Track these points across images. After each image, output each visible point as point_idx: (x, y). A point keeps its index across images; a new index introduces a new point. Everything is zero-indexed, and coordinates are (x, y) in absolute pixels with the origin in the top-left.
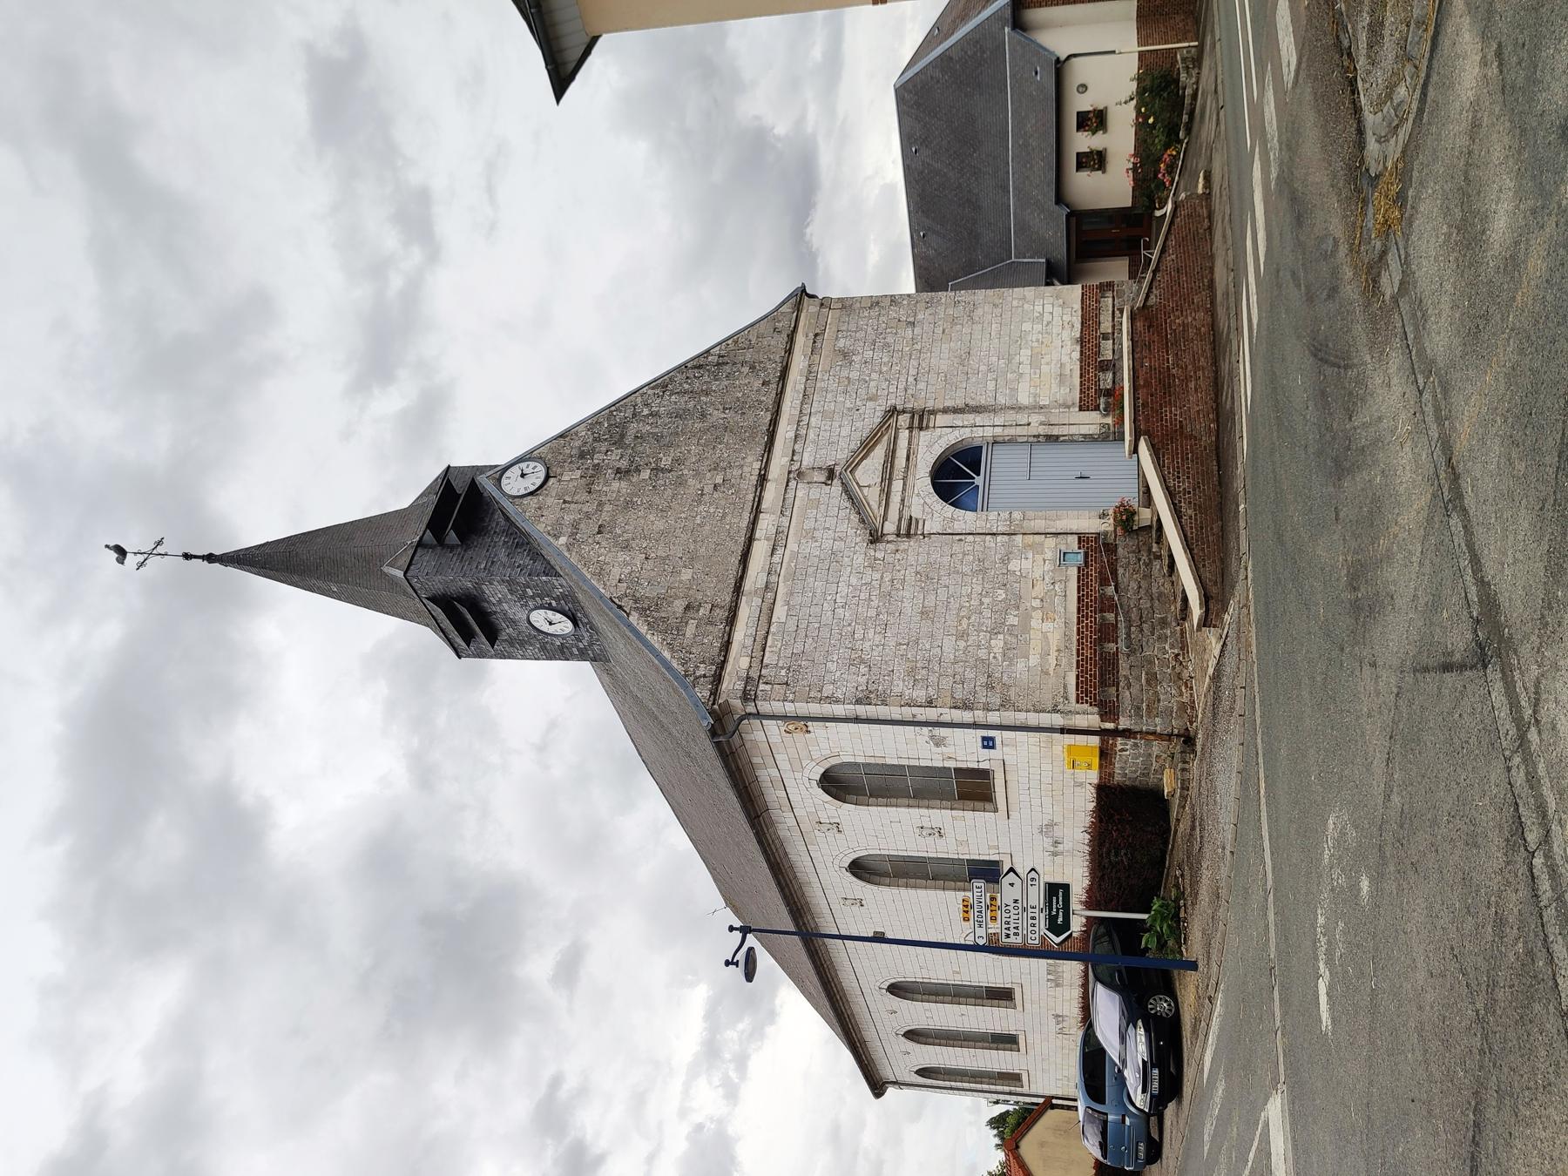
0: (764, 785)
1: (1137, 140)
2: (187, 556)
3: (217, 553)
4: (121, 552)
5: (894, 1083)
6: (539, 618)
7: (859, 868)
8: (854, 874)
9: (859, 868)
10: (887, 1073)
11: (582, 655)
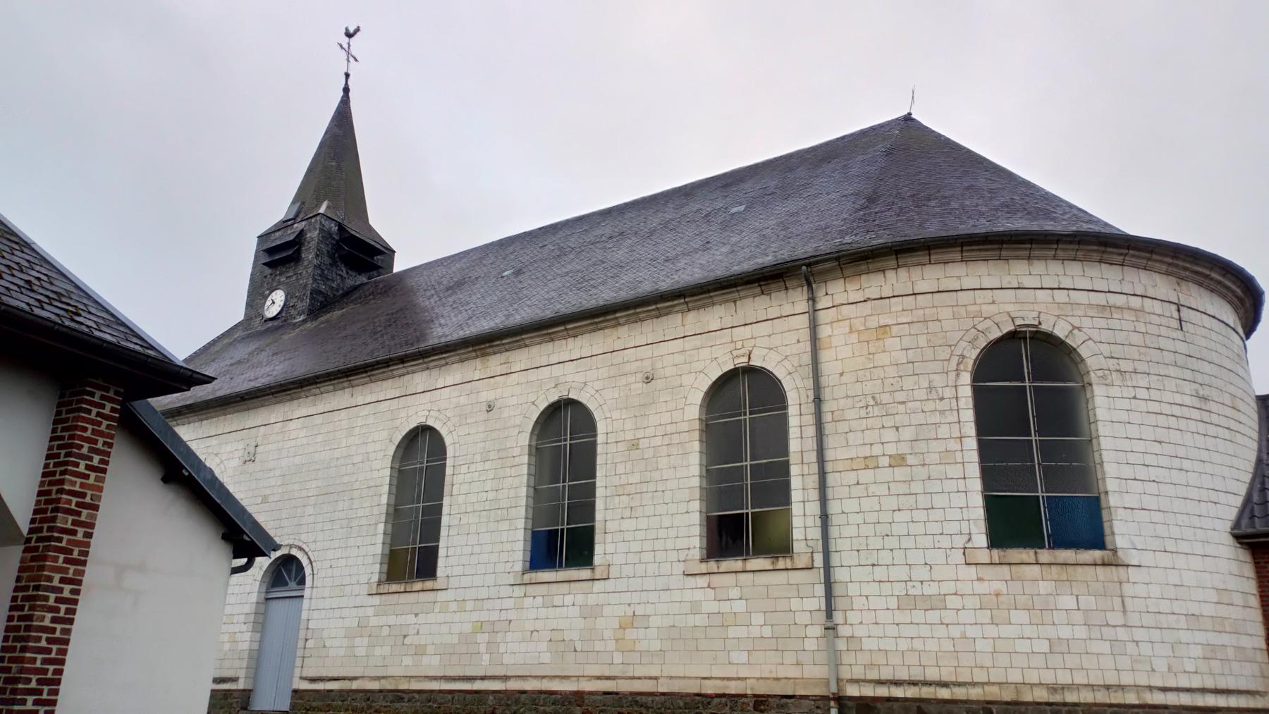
2: (347, 75)
11: (248, 319)
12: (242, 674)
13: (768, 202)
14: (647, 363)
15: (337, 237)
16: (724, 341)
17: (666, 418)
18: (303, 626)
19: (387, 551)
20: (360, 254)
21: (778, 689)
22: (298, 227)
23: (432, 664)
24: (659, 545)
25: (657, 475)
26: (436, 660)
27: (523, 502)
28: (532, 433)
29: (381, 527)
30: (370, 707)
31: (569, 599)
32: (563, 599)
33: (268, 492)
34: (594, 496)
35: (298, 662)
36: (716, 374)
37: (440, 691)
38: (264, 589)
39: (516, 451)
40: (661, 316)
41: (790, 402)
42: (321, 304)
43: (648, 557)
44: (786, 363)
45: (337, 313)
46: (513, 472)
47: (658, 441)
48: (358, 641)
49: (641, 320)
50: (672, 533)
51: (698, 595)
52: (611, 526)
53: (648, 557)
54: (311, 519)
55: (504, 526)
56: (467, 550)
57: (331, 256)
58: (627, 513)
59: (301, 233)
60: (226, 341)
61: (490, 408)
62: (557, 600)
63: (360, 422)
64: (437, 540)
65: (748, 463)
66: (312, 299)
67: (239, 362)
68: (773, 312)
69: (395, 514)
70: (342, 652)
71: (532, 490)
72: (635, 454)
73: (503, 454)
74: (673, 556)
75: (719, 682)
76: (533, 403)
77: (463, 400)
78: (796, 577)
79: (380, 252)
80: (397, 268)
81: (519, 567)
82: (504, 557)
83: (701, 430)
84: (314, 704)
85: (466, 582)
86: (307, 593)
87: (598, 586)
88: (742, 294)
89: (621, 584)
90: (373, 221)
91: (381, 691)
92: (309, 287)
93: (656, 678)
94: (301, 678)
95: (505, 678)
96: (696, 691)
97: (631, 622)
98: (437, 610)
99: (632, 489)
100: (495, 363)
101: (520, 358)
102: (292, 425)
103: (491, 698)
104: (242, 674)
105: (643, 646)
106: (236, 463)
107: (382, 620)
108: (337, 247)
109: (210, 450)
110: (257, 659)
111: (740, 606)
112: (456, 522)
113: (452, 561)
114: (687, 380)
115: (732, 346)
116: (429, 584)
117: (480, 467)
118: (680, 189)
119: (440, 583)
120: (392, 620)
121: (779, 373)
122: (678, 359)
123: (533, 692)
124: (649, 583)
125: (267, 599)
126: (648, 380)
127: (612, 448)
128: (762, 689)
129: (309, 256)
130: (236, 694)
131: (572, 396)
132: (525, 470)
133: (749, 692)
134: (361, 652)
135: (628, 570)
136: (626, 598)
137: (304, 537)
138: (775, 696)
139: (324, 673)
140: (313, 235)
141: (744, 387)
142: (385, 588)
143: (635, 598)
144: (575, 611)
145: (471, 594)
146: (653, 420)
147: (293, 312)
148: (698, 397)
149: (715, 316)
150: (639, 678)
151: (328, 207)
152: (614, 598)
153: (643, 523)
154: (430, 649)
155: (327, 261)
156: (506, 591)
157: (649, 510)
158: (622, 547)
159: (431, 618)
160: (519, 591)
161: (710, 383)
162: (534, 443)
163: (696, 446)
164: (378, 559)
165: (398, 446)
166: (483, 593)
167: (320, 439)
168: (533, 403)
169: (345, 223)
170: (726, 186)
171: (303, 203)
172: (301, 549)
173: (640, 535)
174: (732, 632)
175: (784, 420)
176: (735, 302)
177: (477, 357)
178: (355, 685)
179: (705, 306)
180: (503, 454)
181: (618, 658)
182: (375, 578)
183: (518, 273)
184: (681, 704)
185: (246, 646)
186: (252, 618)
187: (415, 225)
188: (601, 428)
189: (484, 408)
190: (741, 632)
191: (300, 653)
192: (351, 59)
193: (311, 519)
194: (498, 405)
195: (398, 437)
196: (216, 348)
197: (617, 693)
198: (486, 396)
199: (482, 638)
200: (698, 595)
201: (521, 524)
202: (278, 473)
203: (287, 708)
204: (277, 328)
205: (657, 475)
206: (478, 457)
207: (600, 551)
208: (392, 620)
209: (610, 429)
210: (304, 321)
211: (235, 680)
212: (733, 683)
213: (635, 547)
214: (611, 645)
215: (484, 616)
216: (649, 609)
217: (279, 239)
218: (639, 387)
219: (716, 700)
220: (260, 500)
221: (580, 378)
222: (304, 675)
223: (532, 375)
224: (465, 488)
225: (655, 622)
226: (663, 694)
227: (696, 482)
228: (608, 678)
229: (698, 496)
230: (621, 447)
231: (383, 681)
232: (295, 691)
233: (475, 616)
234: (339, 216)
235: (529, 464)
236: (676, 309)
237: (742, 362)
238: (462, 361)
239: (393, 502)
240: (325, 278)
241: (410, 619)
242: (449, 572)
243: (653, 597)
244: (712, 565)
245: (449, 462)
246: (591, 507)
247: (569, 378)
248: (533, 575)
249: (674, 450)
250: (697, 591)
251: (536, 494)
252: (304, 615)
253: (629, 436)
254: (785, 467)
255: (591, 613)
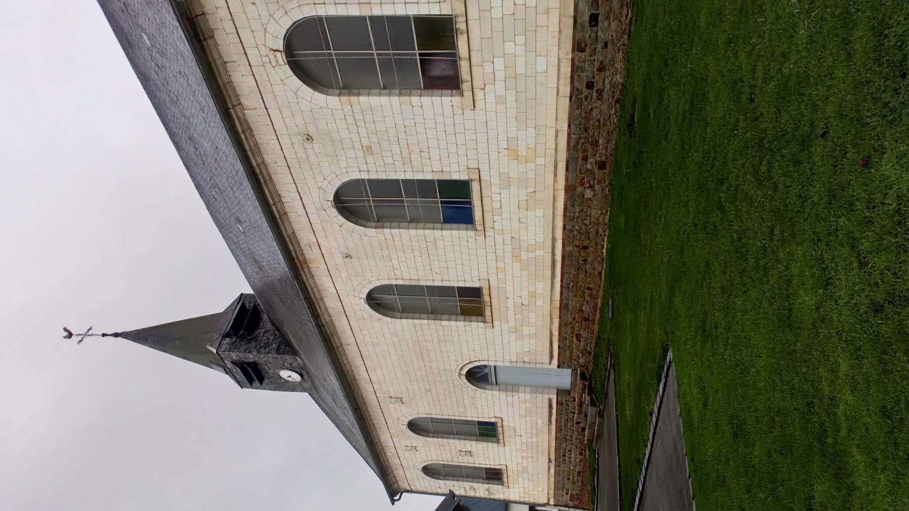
1: (584, 91)
2: (104, 335)
3: (120, 332)
4: (70, 335)
5: (407, 491)
6: (285, 374)
8: (425, 473)
9: (415, 426)
10: (403, 484)
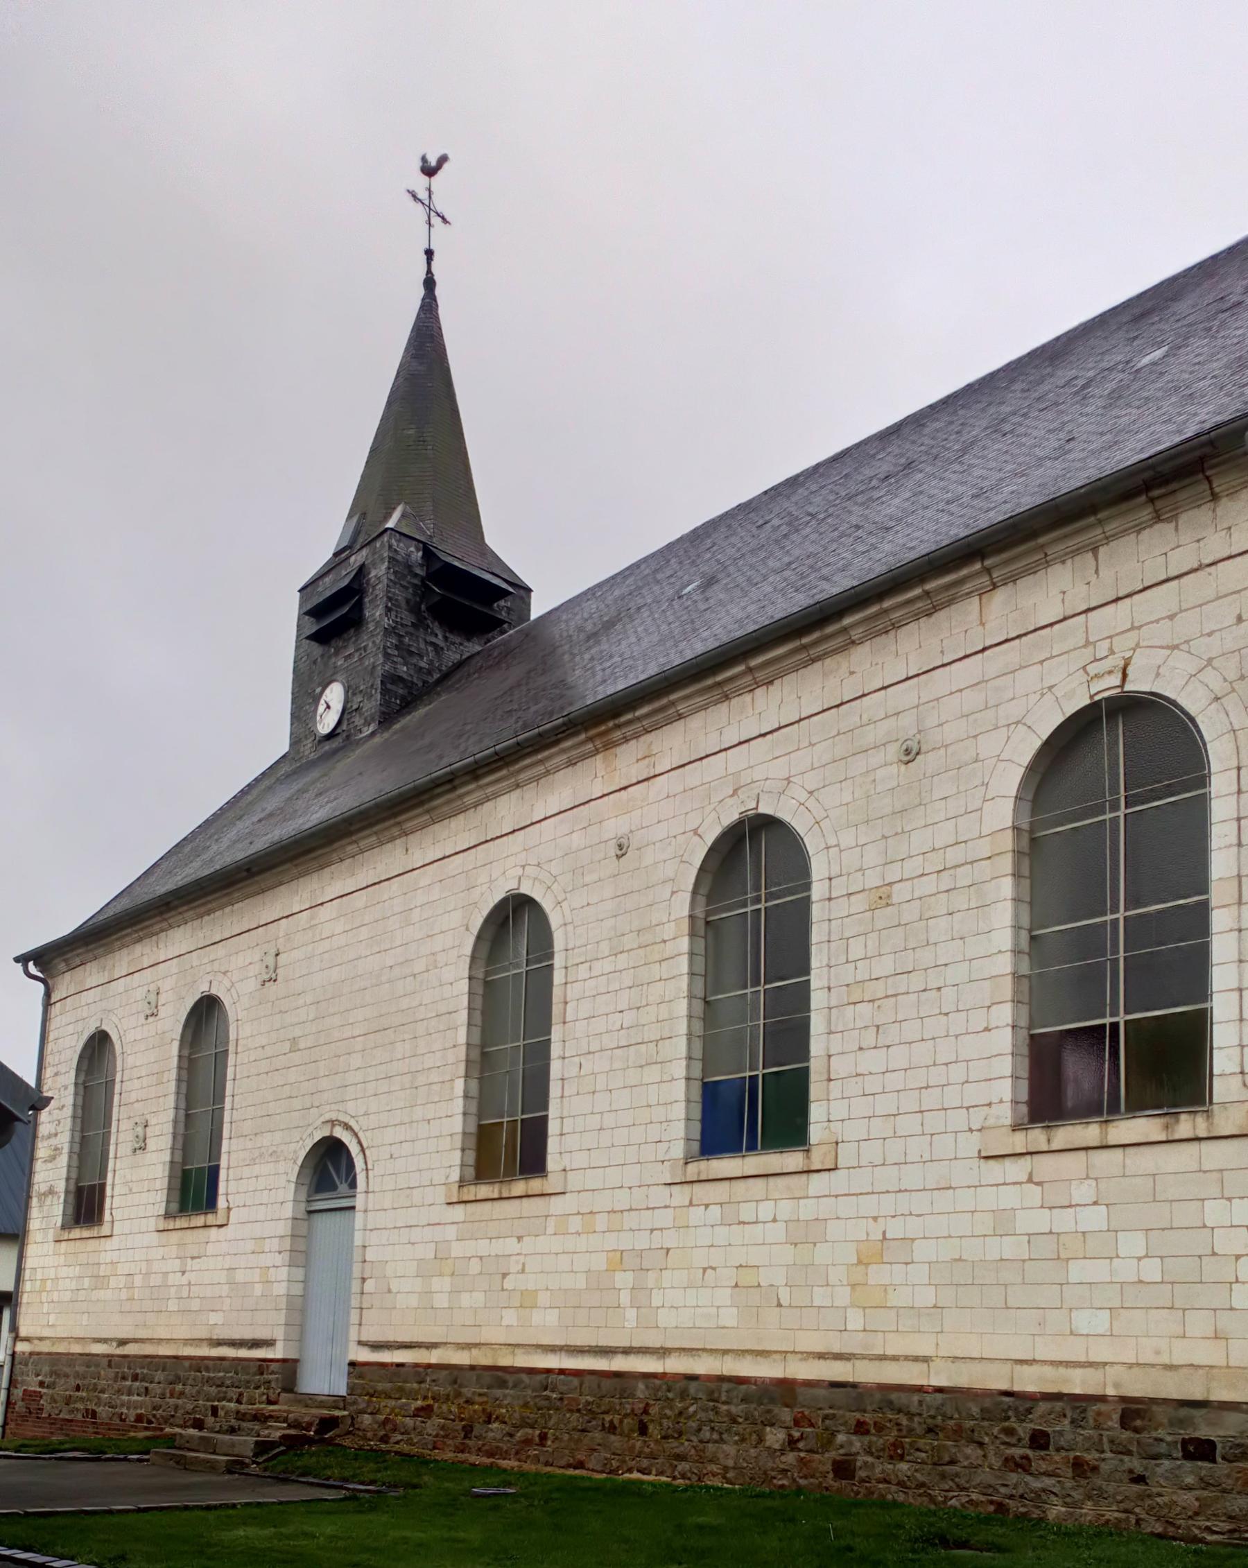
0: (138, 949)
2: (429, 253)
3: (437, 292)
6: (335, 695)
7: (206, 1012)
9: (206, 1012)
11: (295, 741)
12: (279, 1333)
13: (1223, 324)
14: (907, 720)
15: (421, 572)
16: (1070, 643)
17: (945, 834)
18: (357, 1256)
19: (473, 1129)
20: (464, 601)
21: (1172, 1388)
22: (356, 560)
23: (546, 1324)
24: (931, 1099)
25: (926, 957)
26: (551, 1317)
27: (682, 1028)
28: (695, 892)
29: (459, 1085)
30: (458, 1395)
31: (766, 1211)
32: (759, 1202)
33: (297, 1032)
34: (807, 1008)
35: (354, 1317)
36: (1049, 721)
37: (562, 1372)
38: (303, 1197)
39: (669, 931)
40: (935, 609)
41: (1215, 766)
42: (400, 698)
43: (908, 1124)
44: (1210, 676)
45: (421, 712)
46: (664, 970)
47: (928, 886)
48: (436, 1283)
49: (896, 626)
50: (957, 1073)
51: (1009, 1198)
52: (840, 1066)
53: (908, 1124)
54: (359, 1076)
55: (652, 1074)
56: (594, 1121)
57: (414, 609)
58: (869, 1038)
59: (362, 571)
60: (266, 783)
61: (622, 850)
62: (747, 1212)
63: (420, 898)
64: (545, 1107)
65: (1121, 915)
66: (385, 692)
67: (271, 815)
68: (1181, 560)
69: (482, 1063)
70: (413, 1301)
71: (699, 1006)
72: (885, 916)
73: (646, 938)
74: (958, 1120)
75: (1048, 1370)
76: (695, 831)
77: (577, 840)
78: (1215, 1154)
79: (504, 594)
80: (536, 612)
81: (678, 1151)
82: (654, 1132)
83: (1018, 854)
84: (380, 1386)
85: (593, 1179)
86: (359, 1202)
87: (817, 1183)
88: (1111, 527)
89: (861, 1180)
90: (492, 539)
91: (472, 1368)
92: (379, 671)
93: (926, 1359)
94: (360, 1343)
95: (663, 1352)
96: (1004, 1386)
97: (875, 1253)
98: (550, 1230)
99: (879, 989)
100: (627, 760)
101: (671, 743)
102: (325, 913)
103: (641, 1386)
104: (279, 1333)
105: (897, 1298)
106: (252, 985)
107: (470, 1248)
108: (423, 590)
109: (216, 966)
110: (299, 1311)
111: (1094, 1219)
112: (574, 1071)
113: (571, 1142)
114: (989, 746)
115: (1087, 654)
116: (535, 1185)
117: (607, 966)
118: (1044, 348)
119: (552, 1182)
120: (483, 1247)
121: (1192, 701)
122: (973, 699)
123: (709, 1378)
124: (912, 1177)
125: (310, 1212)
126: (910, 755)
127: (839, 909)
128: (1138, 1387)
129: (375, 612)
130: (273, 1366)
131: (764, 809)
132: (683, 965)
133: (1110, 1391)
134: (441, 1301)
135: (871, 1152)
136: (869, 1205)
137: (351, 1107)
138: (1166, 1401)
139: (390, 1337)
140: (380, 572)
141: (1115, 745)
142: (470, 1192)
143: (887, 1204)
144: (777, 1232)
145: (603, 1202)
146: (920, 841)
147: (358, 721)
148: (1010, 779)
149: (1051, 591)
150: (895, 1358)
151: (404, 516)
152: (845, 1207)
153: (899, 1057)
154: (543, 1298)
155: (408, 618)
156: (660, 1195)
157: (911, 1030)
158: (861, 1107)
159: (542, 1244)
160: (680, 1195)
161: (1038, 743)
162: (700, 912)
163: (1007, 887)
164: (458, 1143)
165: (479, 938)
166: (622, 1199)
167: (364, 933)
168: (695, 831)
169: (436, 542)
170: (1137, 319)
171: (364, 515)
172: (347, 1127)
173: (895, 1081)
174: (1077, 1271)
175: (1201, 806)
176: (1095, 550)
177: (597, 752)
178: (434, 1357)
179: (1031, 571)
180: (646, 938)
181: (855, 1321)
182: (455, 1175)
183: (710, 582)
184: (975, 1410)
185: (281, 1289)
186: (287, 1244)
187: (554, 531)
188: (818, 869)
189: (613, 850)
190: (1097, 1271)
191: (354, 1302)
192: (436, 221)
193: (359, 1076)
194: (635, 842)
195: (478, 921)
196: (255, 792)
197: (854, 1386)
198: (614, 827)
199: (624, 1279)
200: (1009, 1198)
201: (679, 1069)
202: (309, 998)
203: (343, 1391)
204: (335, 752)
205: (926, 957)
206: (605, 948)
207: (821, 1116)
208: (483, 1247)
209: (835, 870)
210: (373, 734)
211: (269, 1343)
212: (1078, 1372)
213: (885, 1104)
214: (843, 1296)
215: (626, 1242)
216: (913, 1227)
217: (329, 588)
218: (892, 774)
219: (1043, 1407)
220: (287, 1046)
221: (778, 769)
222: (364, 1339)
223: (693, 775)
224: (585, 1009)
225: (923, 1251)
226: (940, 1390)
227: (1004, 964)
228: (838, 1357)
229: (1008, 994)
230: (859, 903)
231: (475, 1351)
232: (352, 1364)
233: (611, 1242)
234: (426, 530)
235: (692, 954)
236: (967, 587)
237: (1107, 686)
238: (571, 763)
239: (476, 1039)
240: (406, 652)
241: (511, 1245)
242: (566, 1162)
243: (920, 1203)
244: (1037, 1137)
245: (558, 961)
246: (801, 1031)
247: (758, 774)
248: (703, 1164)
249: (960, 901)
250: (1007, 1188)
251: (708, 1013)
252: (358, 1240)
253: (873, 880)
254: (1203, 911)
255: (805, 1235)
